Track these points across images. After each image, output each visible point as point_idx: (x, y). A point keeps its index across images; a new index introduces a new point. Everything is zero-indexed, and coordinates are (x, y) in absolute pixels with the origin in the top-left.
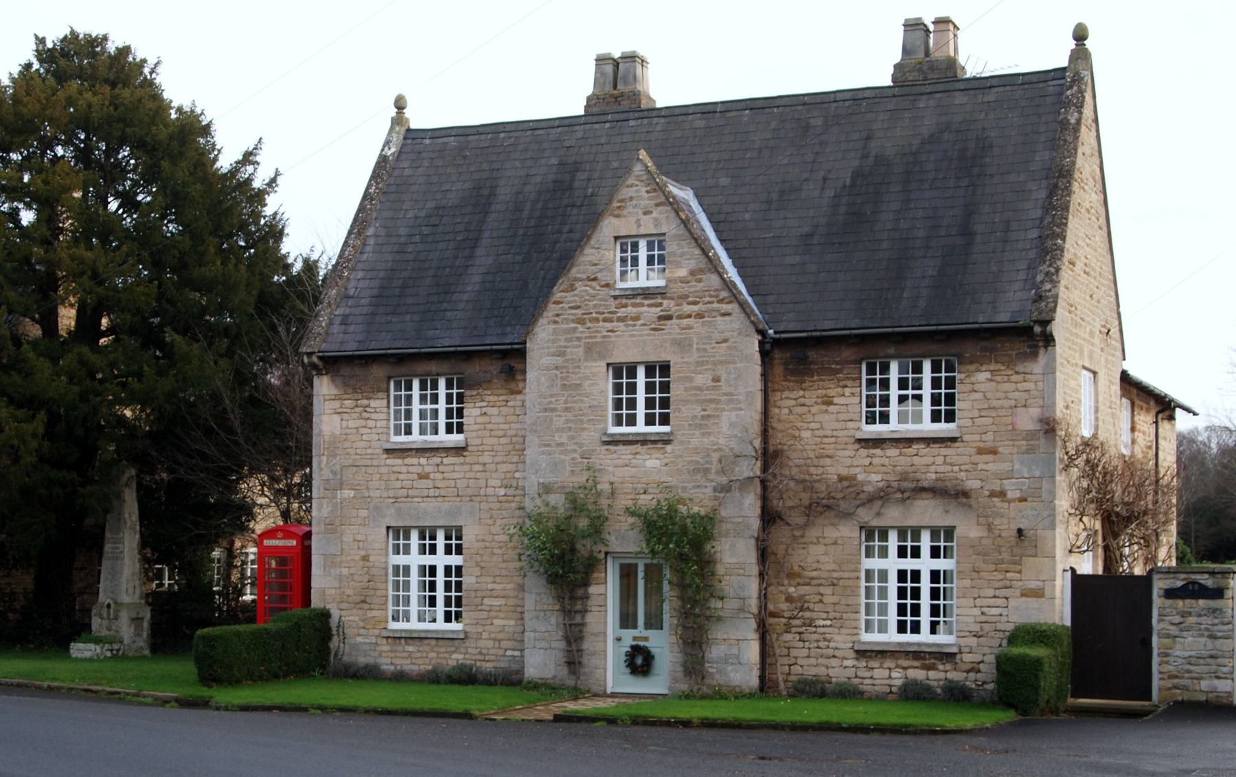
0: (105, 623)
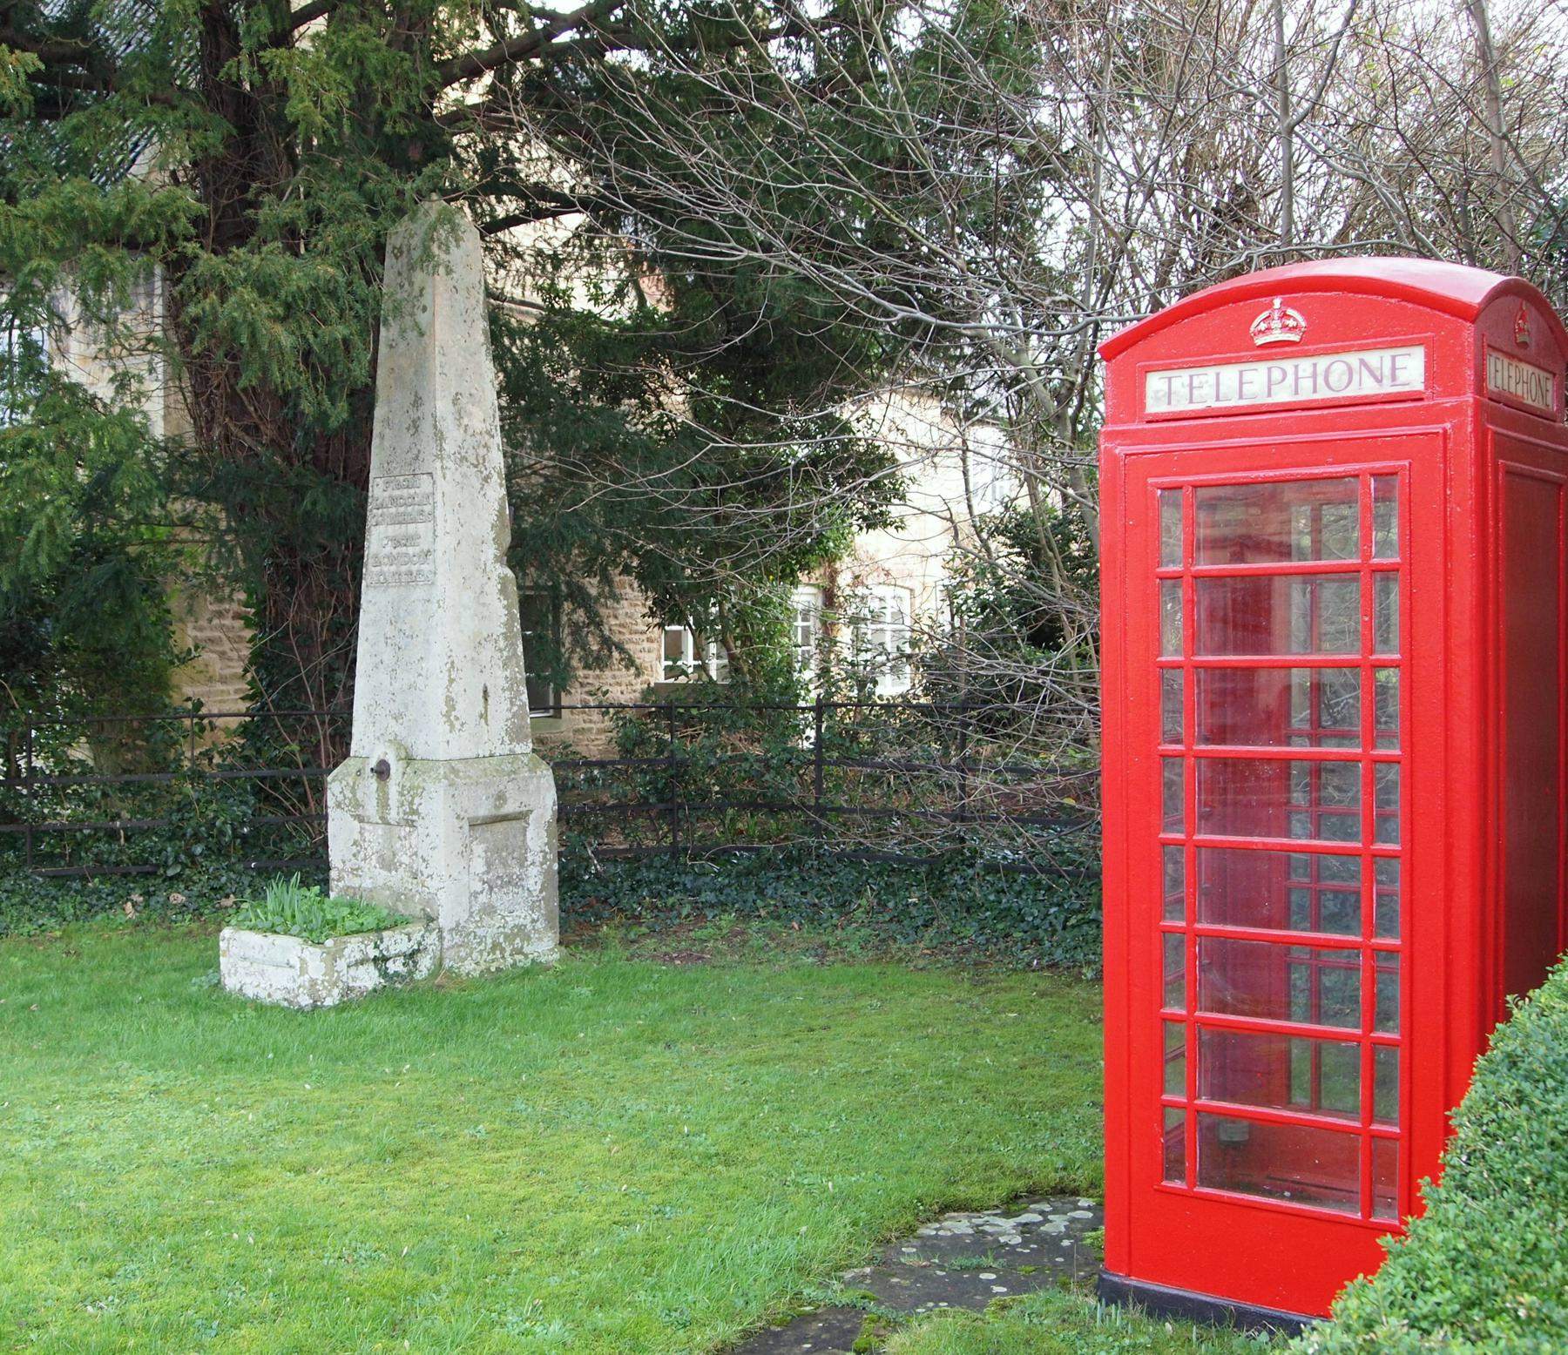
0: (375, 836)
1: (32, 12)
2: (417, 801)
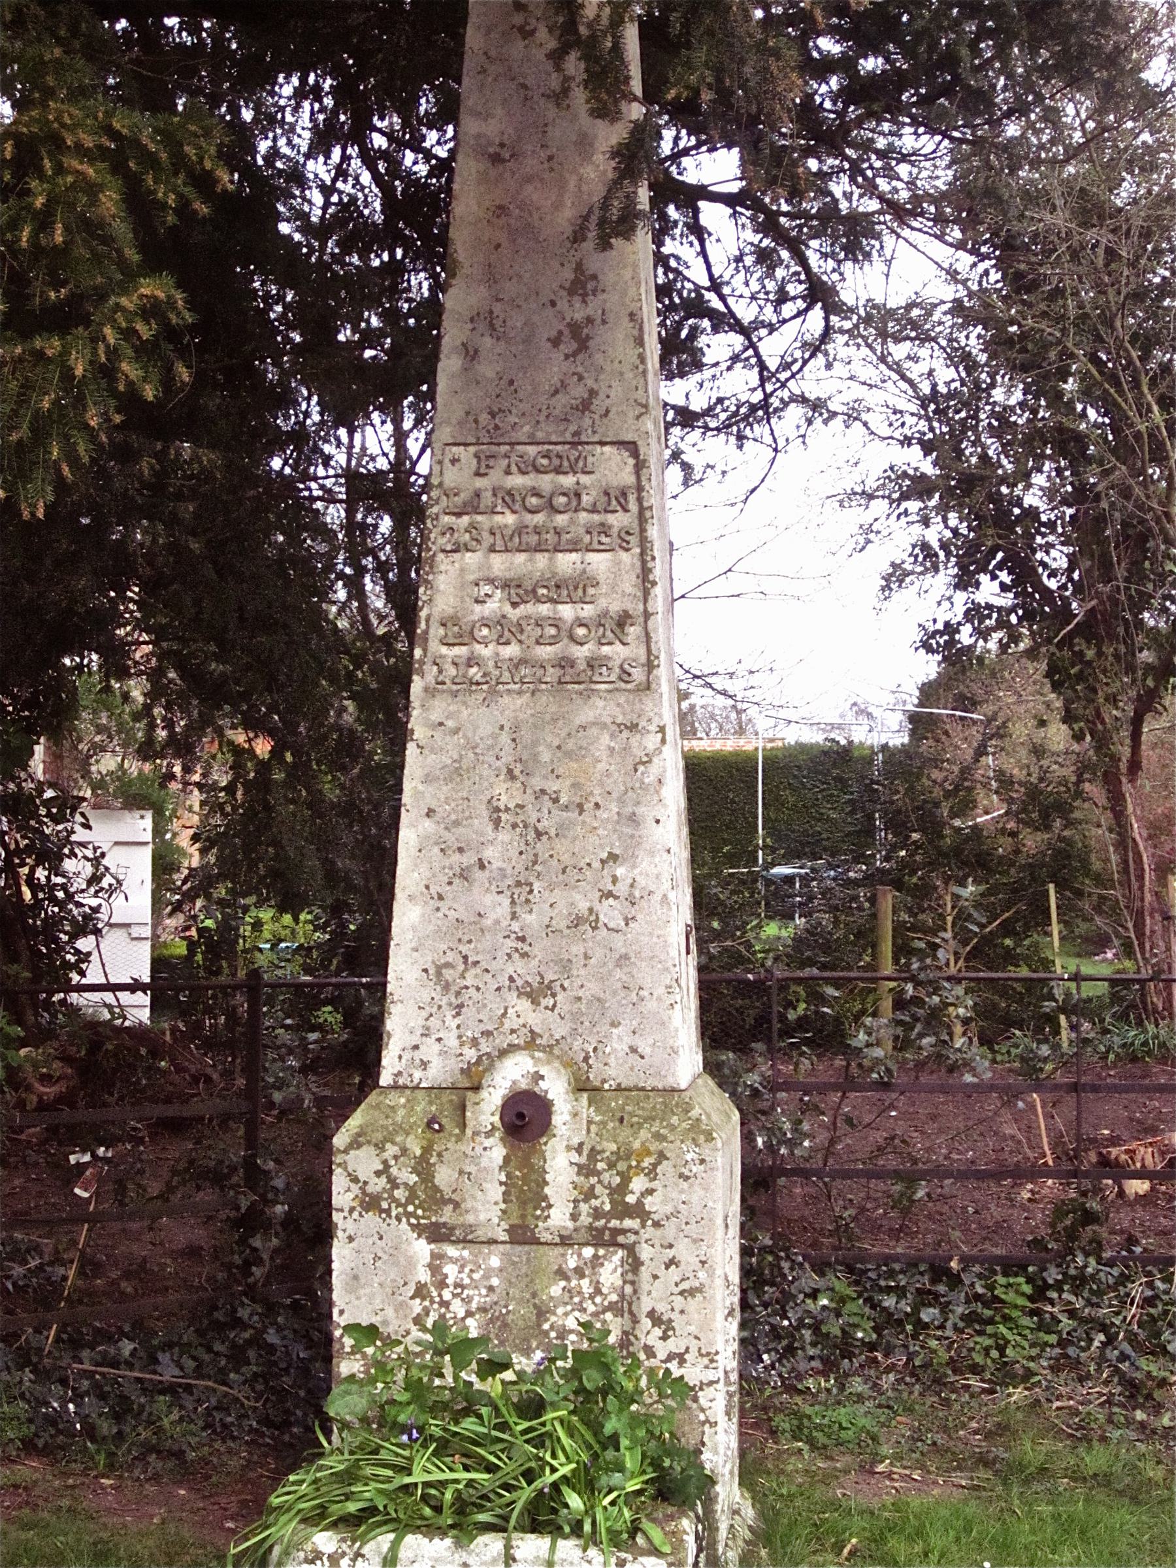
1: (10, 133)
2: (638, 1184)
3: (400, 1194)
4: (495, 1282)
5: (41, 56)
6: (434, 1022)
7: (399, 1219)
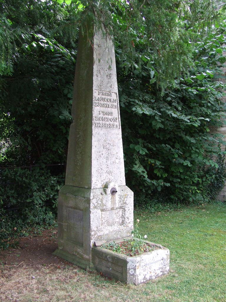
3: (99, 205)
4: (108, 216)
5: (188, 89)
6: (98, 179)
7: (99, 209)
